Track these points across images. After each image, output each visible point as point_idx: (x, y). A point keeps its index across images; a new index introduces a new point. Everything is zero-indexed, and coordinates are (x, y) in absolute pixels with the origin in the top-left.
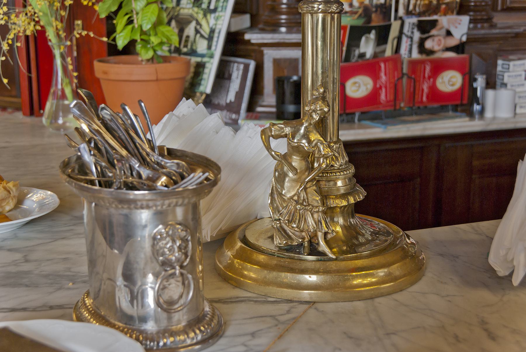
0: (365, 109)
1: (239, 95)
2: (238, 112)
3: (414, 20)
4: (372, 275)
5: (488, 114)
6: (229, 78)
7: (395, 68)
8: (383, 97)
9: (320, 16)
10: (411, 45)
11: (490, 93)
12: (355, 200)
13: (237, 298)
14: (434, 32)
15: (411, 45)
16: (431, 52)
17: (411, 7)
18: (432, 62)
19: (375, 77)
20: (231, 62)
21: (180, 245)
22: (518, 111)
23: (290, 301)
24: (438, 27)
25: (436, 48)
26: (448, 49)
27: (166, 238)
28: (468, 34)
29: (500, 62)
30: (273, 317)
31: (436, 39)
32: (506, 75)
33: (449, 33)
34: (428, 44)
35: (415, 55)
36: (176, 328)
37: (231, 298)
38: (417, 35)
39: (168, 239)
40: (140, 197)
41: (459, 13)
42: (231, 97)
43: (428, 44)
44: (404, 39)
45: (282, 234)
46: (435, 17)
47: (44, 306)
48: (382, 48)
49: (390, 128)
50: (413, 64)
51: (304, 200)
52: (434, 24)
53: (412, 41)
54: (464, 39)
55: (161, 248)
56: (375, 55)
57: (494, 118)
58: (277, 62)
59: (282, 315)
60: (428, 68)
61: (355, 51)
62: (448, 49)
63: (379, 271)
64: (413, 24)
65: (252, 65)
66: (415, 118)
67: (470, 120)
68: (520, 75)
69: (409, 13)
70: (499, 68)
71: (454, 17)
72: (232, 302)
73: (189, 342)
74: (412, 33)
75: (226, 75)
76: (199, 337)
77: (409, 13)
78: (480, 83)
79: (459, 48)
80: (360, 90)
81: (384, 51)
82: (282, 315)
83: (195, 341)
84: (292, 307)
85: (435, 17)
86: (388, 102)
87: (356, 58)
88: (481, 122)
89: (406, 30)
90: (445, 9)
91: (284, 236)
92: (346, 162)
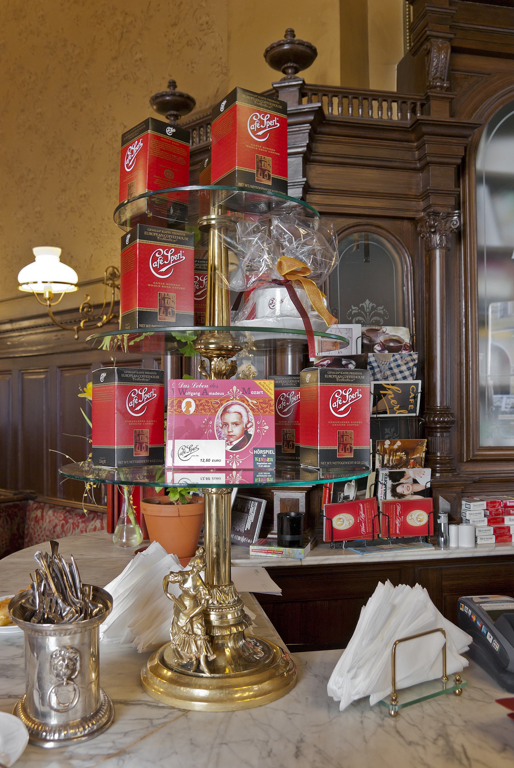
0: (350, 539)
1: (254, 525)
2: (252, 538)
3: (387, 471)
4: (249, 690)
5: (453, 544)
6: (248, 512)
7: (372, 508)
8: (363, 529)
9: (214, 496)
10: (385, 490)
11: (453, 528)
12: (237, 630)
13: (139, 701)
14: (402, 481)
15: (385, 490)
16: (402, 496)
17: (385, 462)
18: (401, 503)
19: (356, 515)
20: (250, 500)
21: (67, 663)
22: (478, 542)
23: (173, 708)
24: (405, 477)
25: (406, 492)
26: (416, 493)
27: (59, 657)
28: (431, 482)
29: (464, 502)
30: (151, 720)
31: (405, 486)
32: (468, 513)
33: (415, 481)
34: (399, 490)
35: (389, 497)
36: (73, 723)
37: (134, 701)
38: (389, 483)
39: (60, 658)
40: (45, 629)
41: (425, 467)
42: (248, 526)
43: (399, 490)
44: (380, 486)
45: (175, 655)
46: (404, 469)
47: (6, 695)
48: (362, 492)
49: (365, 554)
50: (387, 504)
51: (189, 630)
52: (402, 475)
53: (386, 487)
54: (429, 485)
55: (55, 664)
56: (357, 498)
57: (458, 548)
58: (282, 501)
59: (158, 719)
60: (399, 508)
61: (340, 494)
62: (416, 493)
63: (254, 686)
64: (386, 474)
65: (264, 502)
66: (391, 546)
67: (436, 549)
68: (480, 513)
69: (383, 466)
70: (463, 507)
71: (418, 470)
72: (132, 704)
73: (79, 734)
74: (386, 481)
75: (246, 511)
76: (86, 732)
77: (383, 466)
78: (443, 520)
79: (424, 493)
80: (344, 524)
81: (365, 495)
82: (158, 719)
83: (83, 733)
84: (171, 713)
85: (404, 469)
86: (367, 533)
87: (341, 500)
88: (445, 551)
89: (380, 479)
90: (414, 463)
91: (177, 656)
92: (235, 601)
